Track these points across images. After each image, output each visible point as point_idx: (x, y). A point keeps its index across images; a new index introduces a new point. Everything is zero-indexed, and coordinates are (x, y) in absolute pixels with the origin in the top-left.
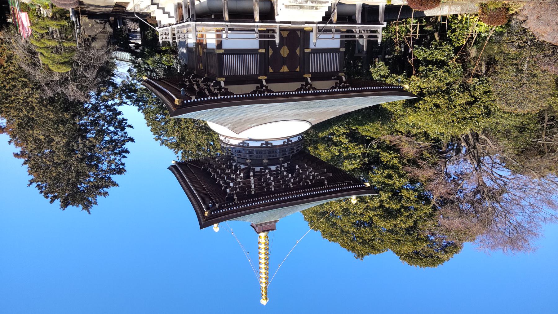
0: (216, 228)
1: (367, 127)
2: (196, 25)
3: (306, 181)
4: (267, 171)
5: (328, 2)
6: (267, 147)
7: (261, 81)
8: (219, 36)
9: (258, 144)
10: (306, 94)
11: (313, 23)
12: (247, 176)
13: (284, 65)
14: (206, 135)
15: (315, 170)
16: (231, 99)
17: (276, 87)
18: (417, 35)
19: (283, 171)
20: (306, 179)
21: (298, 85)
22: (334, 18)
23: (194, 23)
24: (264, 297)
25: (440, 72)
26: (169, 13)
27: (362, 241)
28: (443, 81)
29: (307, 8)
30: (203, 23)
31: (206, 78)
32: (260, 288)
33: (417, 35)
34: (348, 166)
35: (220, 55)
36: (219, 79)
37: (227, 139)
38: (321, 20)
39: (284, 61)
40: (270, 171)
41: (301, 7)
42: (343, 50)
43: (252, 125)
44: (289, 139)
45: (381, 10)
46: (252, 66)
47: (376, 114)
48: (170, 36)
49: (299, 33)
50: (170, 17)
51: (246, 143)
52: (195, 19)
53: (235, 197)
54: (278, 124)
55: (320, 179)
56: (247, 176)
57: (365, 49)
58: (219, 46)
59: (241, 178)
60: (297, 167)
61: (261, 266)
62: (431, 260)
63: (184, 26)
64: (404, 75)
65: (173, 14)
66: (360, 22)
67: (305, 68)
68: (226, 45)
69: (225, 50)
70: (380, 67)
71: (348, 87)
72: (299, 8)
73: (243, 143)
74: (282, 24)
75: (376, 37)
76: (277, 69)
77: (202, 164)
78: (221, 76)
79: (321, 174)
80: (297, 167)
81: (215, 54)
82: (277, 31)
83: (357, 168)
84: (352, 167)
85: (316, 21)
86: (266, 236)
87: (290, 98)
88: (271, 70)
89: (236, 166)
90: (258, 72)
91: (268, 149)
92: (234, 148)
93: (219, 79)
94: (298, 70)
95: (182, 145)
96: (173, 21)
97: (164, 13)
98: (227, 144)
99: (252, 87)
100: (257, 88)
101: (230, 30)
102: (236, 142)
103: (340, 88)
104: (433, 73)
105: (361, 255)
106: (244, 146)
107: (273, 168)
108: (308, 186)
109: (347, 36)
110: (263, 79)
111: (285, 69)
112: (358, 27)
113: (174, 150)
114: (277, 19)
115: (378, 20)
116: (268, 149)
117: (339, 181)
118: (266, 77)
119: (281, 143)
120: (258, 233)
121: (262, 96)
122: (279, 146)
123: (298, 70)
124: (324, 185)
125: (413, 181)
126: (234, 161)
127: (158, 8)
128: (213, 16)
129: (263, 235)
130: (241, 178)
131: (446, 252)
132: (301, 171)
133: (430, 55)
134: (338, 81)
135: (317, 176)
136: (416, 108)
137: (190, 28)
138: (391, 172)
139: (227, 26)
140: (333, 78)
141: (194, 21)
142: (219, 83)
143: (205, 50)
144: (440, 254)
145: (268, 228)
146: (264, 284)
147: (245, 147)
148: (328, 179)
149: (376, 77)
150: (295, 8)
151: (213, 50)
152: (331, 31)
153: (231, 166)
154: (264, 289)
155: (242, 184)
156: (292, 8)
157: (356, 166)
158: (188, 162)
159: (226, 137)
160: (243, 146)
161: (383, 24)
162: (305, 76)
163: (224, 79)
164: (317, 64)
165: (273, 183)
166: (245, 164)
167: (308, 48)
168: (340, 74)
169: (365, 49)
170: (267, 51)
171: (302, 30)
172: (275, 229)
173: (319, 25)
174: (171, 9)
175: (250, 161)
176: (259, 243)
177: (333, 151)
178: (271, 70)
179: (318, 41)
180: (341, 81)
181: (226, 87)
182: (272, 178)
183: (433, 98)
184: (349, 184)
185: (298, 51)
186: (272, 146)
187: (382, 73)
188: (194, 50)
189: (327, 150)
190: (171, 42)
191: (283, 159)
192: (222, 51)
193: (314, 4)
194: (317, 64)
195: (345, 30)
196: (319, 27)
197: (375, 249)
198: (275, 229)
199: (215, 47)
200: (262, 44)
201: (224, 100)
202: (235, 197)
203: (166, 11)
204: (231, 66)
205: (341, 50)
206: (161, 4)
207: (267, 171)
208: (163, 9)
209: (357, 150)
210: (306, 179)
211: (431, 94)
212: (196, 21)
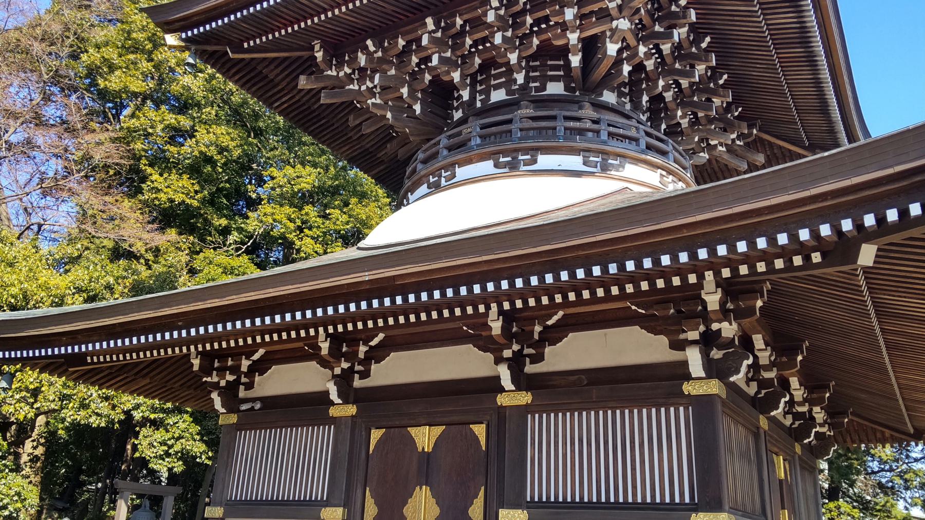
3: (385, 50)
4: (520, 78)
7: (522, 381)
9: (545, 161)
36: (714, 387)
39: (426, 468)
44: (436, 187)
55: (339, 66)
60: (417, 108)
73: (605, 168)
76: (456, 437)
78: (702, 404)
80: (417, 108)
88: (480, 430)
90: (533, 422)
91: (509, 145)
93: (714, 387)
94: (376, 435)
98: (670, 172)
100: (538, 358)
111: (425, 437)
116: (509, 145)
118: (502, 400)
122: (469, 161)
123: (376, 435)
132: (405, 91)
140: (258, 406)
148: (310, 66)
162: (351, 410)
163: (688, 388)
168: (233, 419)
177: (345, 218)
178: (480, 430)
181: (676, 356)
187: (160, 435)
207: (520, 78)
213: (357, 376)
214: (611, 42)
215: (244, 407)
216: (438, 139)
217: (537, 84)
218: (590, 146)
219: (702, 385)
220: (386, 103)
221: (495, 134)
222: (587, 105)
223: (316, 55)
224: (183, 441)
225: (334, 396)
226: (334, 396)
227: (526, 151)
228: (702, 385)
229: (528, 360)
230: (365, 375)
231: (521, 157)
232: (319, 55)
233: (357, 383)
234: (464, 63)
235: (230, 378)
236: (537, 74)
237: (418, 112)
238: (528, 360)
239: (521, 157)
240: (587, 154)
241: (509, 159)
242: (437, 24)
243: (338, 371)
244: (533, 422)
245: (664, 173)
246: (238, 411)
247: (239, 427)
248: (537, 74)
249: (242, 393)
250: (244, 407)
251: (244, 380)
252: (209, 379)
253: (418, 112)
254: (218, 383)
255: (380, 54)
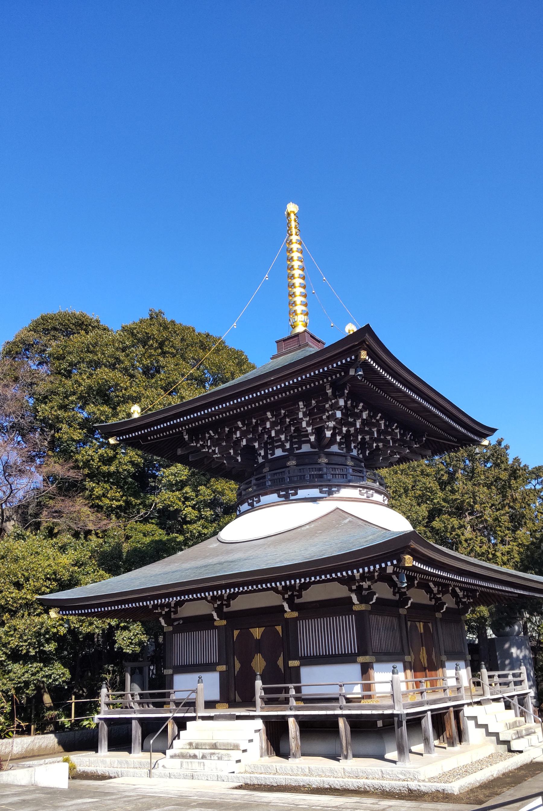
0: (351, 328)
1: (147, 540)
2: (393, 707)
4: (288, 446)
5: (172, 757)
6: (286, 490)
7: (293, 607)
8: (367, 687)
9: (302, 493)
10: (222, 588)
11: (204, 718)
12: (320, 432)
13: (258, 641)
14: (456, 500)
15: (208, 456)
16: (340, 569)
17: (268, 599)
18: (73, 700)
19: (260, 448)
20: (220, 439)
21: (237, 605)
22: (172, 727)
23: (395, 712)
24: (293, 217)
25: (14, 643)
26: (478, 726)
27: (156, 341)
28: (9, 627)
29: (205, 744)
30: (380, 712)
31: (403, 607)
32: (300, 232)
33: (73, 700)
34: (179, 471)
35: (363, 652)
36: (363, 607)
37: (365, 497)
38: (189, 724)
39: (258, 646)
40: (282, 446)
41: (214, 746)
42: (168, 672)
43: (307, 527)
44: (253, 508)
45: (104, 744)
46: (312, 635)
47: (114, 562)
48: (485, 680)
49: (238, 699)
50: (475, 718)
51: (325, 492)
52: (396, 719)
53: (329, 392)
54: (272, 530)
55: (197, 442)
56: (320, 432)
57: (128, 677)
58: (366, 669)
59: (328, 428)
60: (239, 458)
61: (301, 272)
62: (48, 326)
63: (450, 699)
64: (81, 633)
65: (470, 724)
66: (133, 722)
67: (225, 634)
68: (354, 669)
69: (355, 661)
70: (131, 643)
71: (155, 607)
72: (218, 745)
73: (330, 493)
74: (252, 713)
75: (266, 690)
76: (269, 633)
77: (425, 446)
78: (359, 615)
79: (197, 450)
80: (239, 458)
81: (374, 654)
82: (258, 701)
83: (165, 468)
84: (173, 469)
85: (199, 722)
86: (294, 327)
87: (224, 582)
88: (279, 628)
89: (349, 450)
90: (300, 624)
91: (293, 485)
92: (350, 481)
93: (363, 607)
94: (236, 633)
95: (504, 476)
96: (468, 711)
97: (486, 726)
99: (310, 595)
101: (336, 700)
102: (345, 492)
103: (168, 605)
104: (25, 641)
105: (154, 317)
106: (328, 485)
107: (279, 452)
108: (242, 417)
109: (163, 695)
110: (290, 614)
111: (257, 633)
112: (136, 714)
113: (519, 464)
114: (259, 724)
115: (108, 726)
116: (293, 485)
117: (160, 439)
119: (265, 499)
120: (305, 331)
121: (291, 579)
122: (266, 494)
123: (236, 633)
124: (188, 431)
125: (66, 454)
126: (353, 458)
127: (497, 735)
128: (380, 724)
129: (300, 329)
130: (328, 428)
131: (23, 342)
132: (232, 451)
133: (38, 672)
134: (173, 616)
135: (203, 446)
136: (55, 580)
137: (403, 701)
138: (105, 468)
139: (341, 708)
141: (397, 715)
142: (363, 600)
143: (408, 658)
144: (32, 337)
145: (294, 340)
146: (294, 241)
147: (327, 486)
148: (182, 443)
149: (137, 628)
150: (224, 744)
151: (378, 661)
152: (177, 704)
153: (362, 446)
154: (294, 231)
155: (324, 417)
156: (228, 744)
157: (167, 471)
158: (454, 447)
159: (368, 501)
160: (330, 486)
161: (100, 719)
162: (224, 622)
164: (207, 644)
165: (301, 415)
166: (329, 455)
167: (221, 673)
168: (171, 629)
169: (128, 677)
170: (286, 664)
171: (233, 704)
172: (277, 342)
173: (193, 715)
174: (473, 733)
175: (320, 461)
176: (307, 314)
177: (209, 491)
178: (279, 628)
179: (208, 685)
180: (167, 617)
182: (304, 424)
183: (23, 599)
184: (144, 437)
185: (238, 665)
186: (277, 491)
187: (126, 634)
188: (444, 658)
189: (219, 493)
190: (484, 672)
191: (289, 464)
192: (361, 659)
193: (192, 752)
194: (207, 644)
195: (166, 707)
196: (195, 711)
197: (130, 331)
198: (277, 342)
199: (376, 666)
200: (294, 676)
201: (347, 567)
202: (329, 392)
203: (483, 730)
204: (343, 633)
205: (170, 672)
206: (492, 742)
207: (288, 446)
208: (489, 734)
209: (165, 498)
210: (220, 439)
211: (28, 605)
212: (392, 716)
213: (225, 607)
214: (327, 431)
215: (175, 623)
216: (250, 479)
217: (296, 446)
218: (322, 484)
219: (358, 606)
220: (223, 456)
221: (279, 473)
222: (322, 455)
223: (185, 437)
224: (138, 636)
225: (215, 617)
226: (215, 617)
227: (292, 489)
228: (358, 606)
229: (296, 597)
230: (228, 605)
231: (290, 492)
232: (186, 437)
233: (225, 609)
234: (259, 438)
235: (167, 610)
236: (296, 440)
237: (240, 460)
238: (296, 597)
239: (290, 492)
240: (321, 488)
241: (284, 493)
242: (244, 424)
243: (216, 606)
244: (300, 624)
245: (361, 489)
246: (172, 625)
247: (173, 632)
248: (296, 440)
249: (173, 616)
250: (175, 623)
251: (172, 609)
252: (157, 611)
253: (240, 460)
254: (161, 612)
255: (217, 436)
